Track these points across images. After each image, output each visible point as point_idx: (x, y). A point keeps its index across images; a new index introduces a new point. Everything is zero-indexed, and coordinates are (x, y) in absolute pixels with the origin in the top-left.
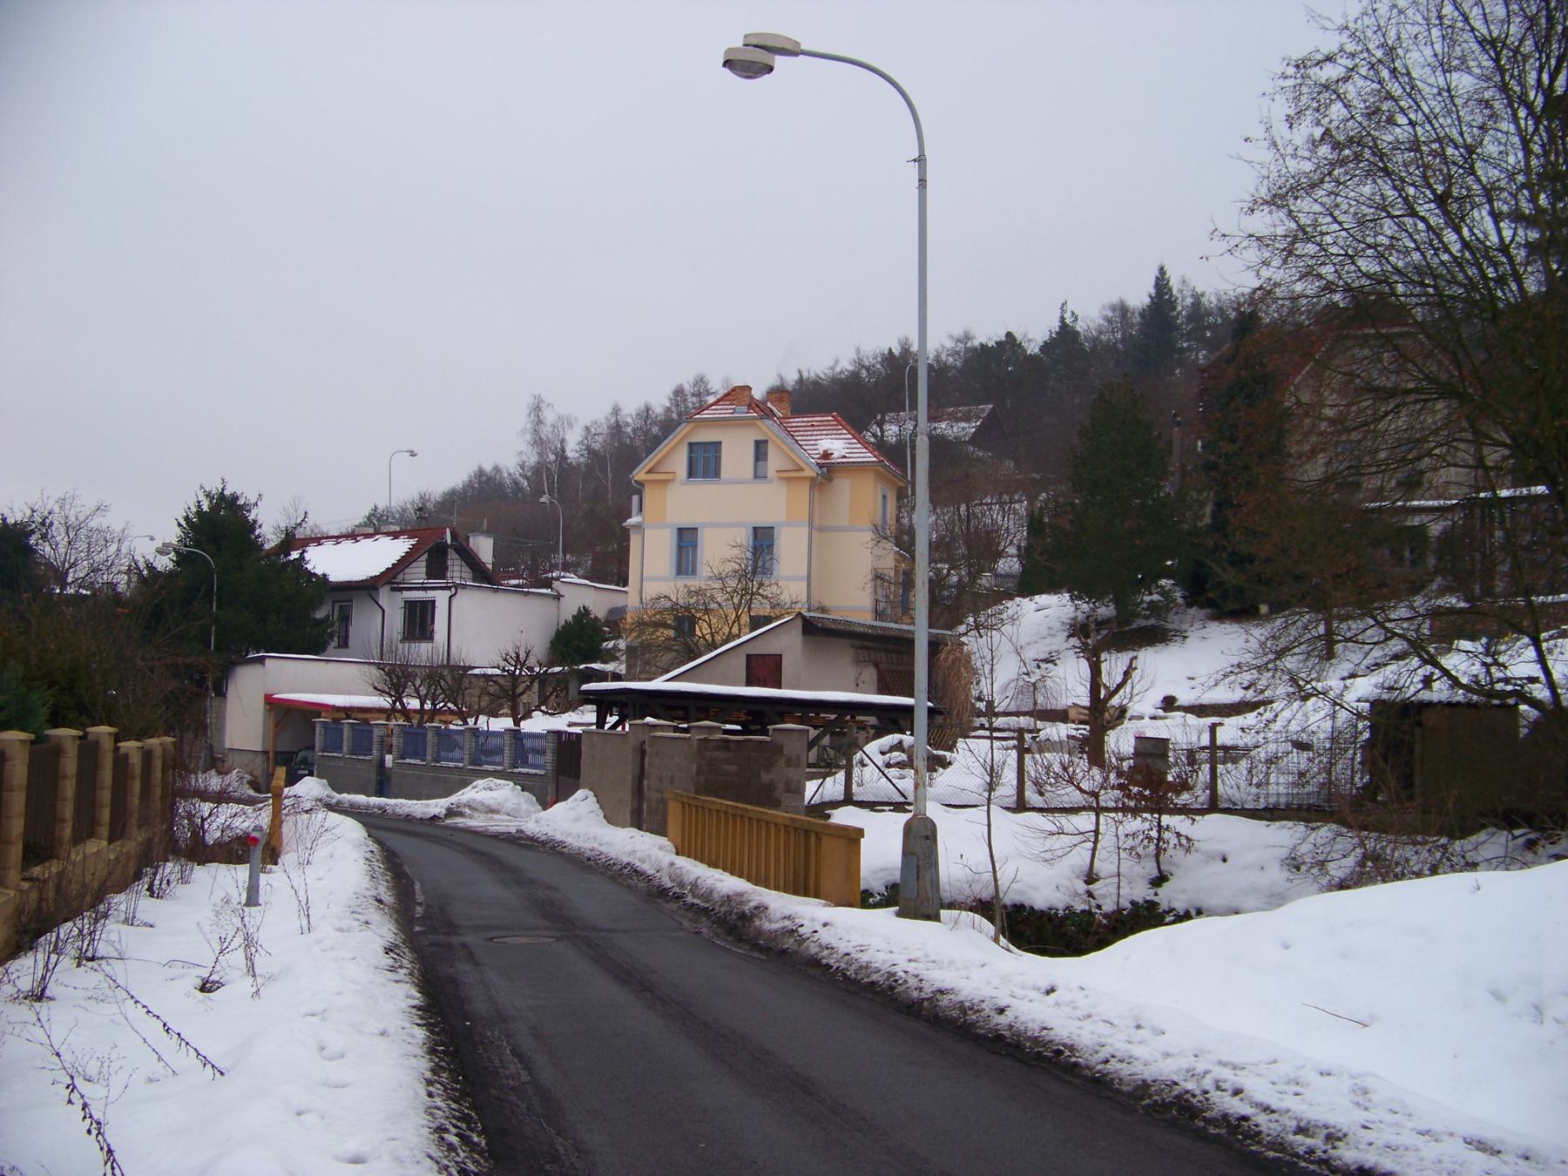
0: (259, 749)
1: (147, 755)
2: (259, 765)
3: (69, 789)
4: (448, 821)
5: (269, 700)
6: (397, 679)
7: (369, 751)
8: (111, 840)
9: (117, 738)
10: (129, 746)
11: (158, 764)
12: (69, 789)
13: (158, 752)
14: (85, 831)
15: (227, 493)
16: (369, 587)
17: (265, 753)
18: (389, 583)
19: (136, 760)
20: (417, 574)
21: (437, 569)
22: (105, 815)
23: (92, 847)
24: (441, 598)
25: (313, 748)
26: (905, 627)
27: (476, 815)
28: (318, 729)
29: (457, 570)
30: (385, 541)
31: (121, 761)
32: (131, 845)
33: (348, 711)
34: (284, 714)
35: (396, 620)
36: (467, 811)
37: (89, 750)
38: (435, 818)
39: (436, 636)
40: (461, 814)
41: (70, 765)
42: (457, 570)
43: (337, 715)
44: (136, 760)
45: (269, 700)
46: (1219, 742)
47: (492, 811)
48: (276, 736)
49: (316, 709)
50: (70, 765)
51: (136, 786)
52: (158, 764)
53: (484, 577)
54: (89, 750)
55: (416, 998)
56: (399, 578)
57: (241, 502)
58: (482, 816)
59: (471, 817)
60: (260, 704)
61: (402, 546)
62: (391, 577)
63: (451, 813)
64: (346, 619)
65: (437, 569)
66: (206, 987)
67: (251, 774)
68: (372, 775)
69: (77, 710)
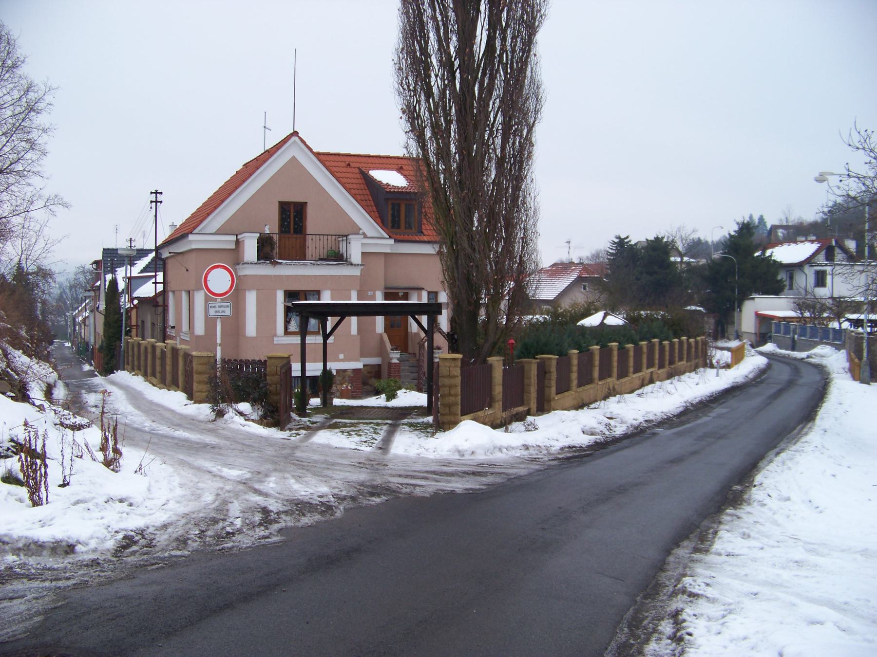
0: (753, 332)
1: (697, 342)
2: (753, 338)
3: (677, 351)
4: (807, 360)
5: (757, 315)
6: (800, 306)
7: (789, 334)
8: (687, 361)
9: (688, 340)
10: (691, 340)
11: (700, 344)
12: (677, 351)
13: (700, 341)
14: (681, 359)
15: (745, 222)
16: (800, 266)
17: (756, 333)
18: (809, 263)
19: (693, 344)
20: (821, 258)
21: (830, 257)
22: (657, 362)
23: (682, 363)
24: (828, 269)
25: (771, 332)
26: (615, 370)
27: (817, 357)
28: (773, 326)
29: (839, 256)
30: (808, 244)
31: (689, 344)
32: (693, 362)
33: (784, 319)
34: (763, 320)
35: (811, 280)
36: (814, 356)
37: (681, 343)
38: (803, 359)
39: (827, 285)
40: (812, 357)
41: (677, 346)
42: (839, 256)
43: (780, 320)
44: (693, 344)
45: (757, 315)
46: (308, 374)
47: (822, 356)
48: (760, 327)
49: (772, 318)
50: (677, 346)
51: (693, 350)
52: (700, 344)
53: (852, 258)
54: (681, 343)
55: (585, 326)
56: (812, 261)
57: (752, 226)
58: (819, 358)
59: (815, 358)
60: (753, 315)
61: (814, 247)
62: (809, 261)
63: (808, 357)
64: (791, 278)
65: (830, 257)
66: (697, 384)
67: (750, 341)
68: (790, 342)
69: (677, 335)
